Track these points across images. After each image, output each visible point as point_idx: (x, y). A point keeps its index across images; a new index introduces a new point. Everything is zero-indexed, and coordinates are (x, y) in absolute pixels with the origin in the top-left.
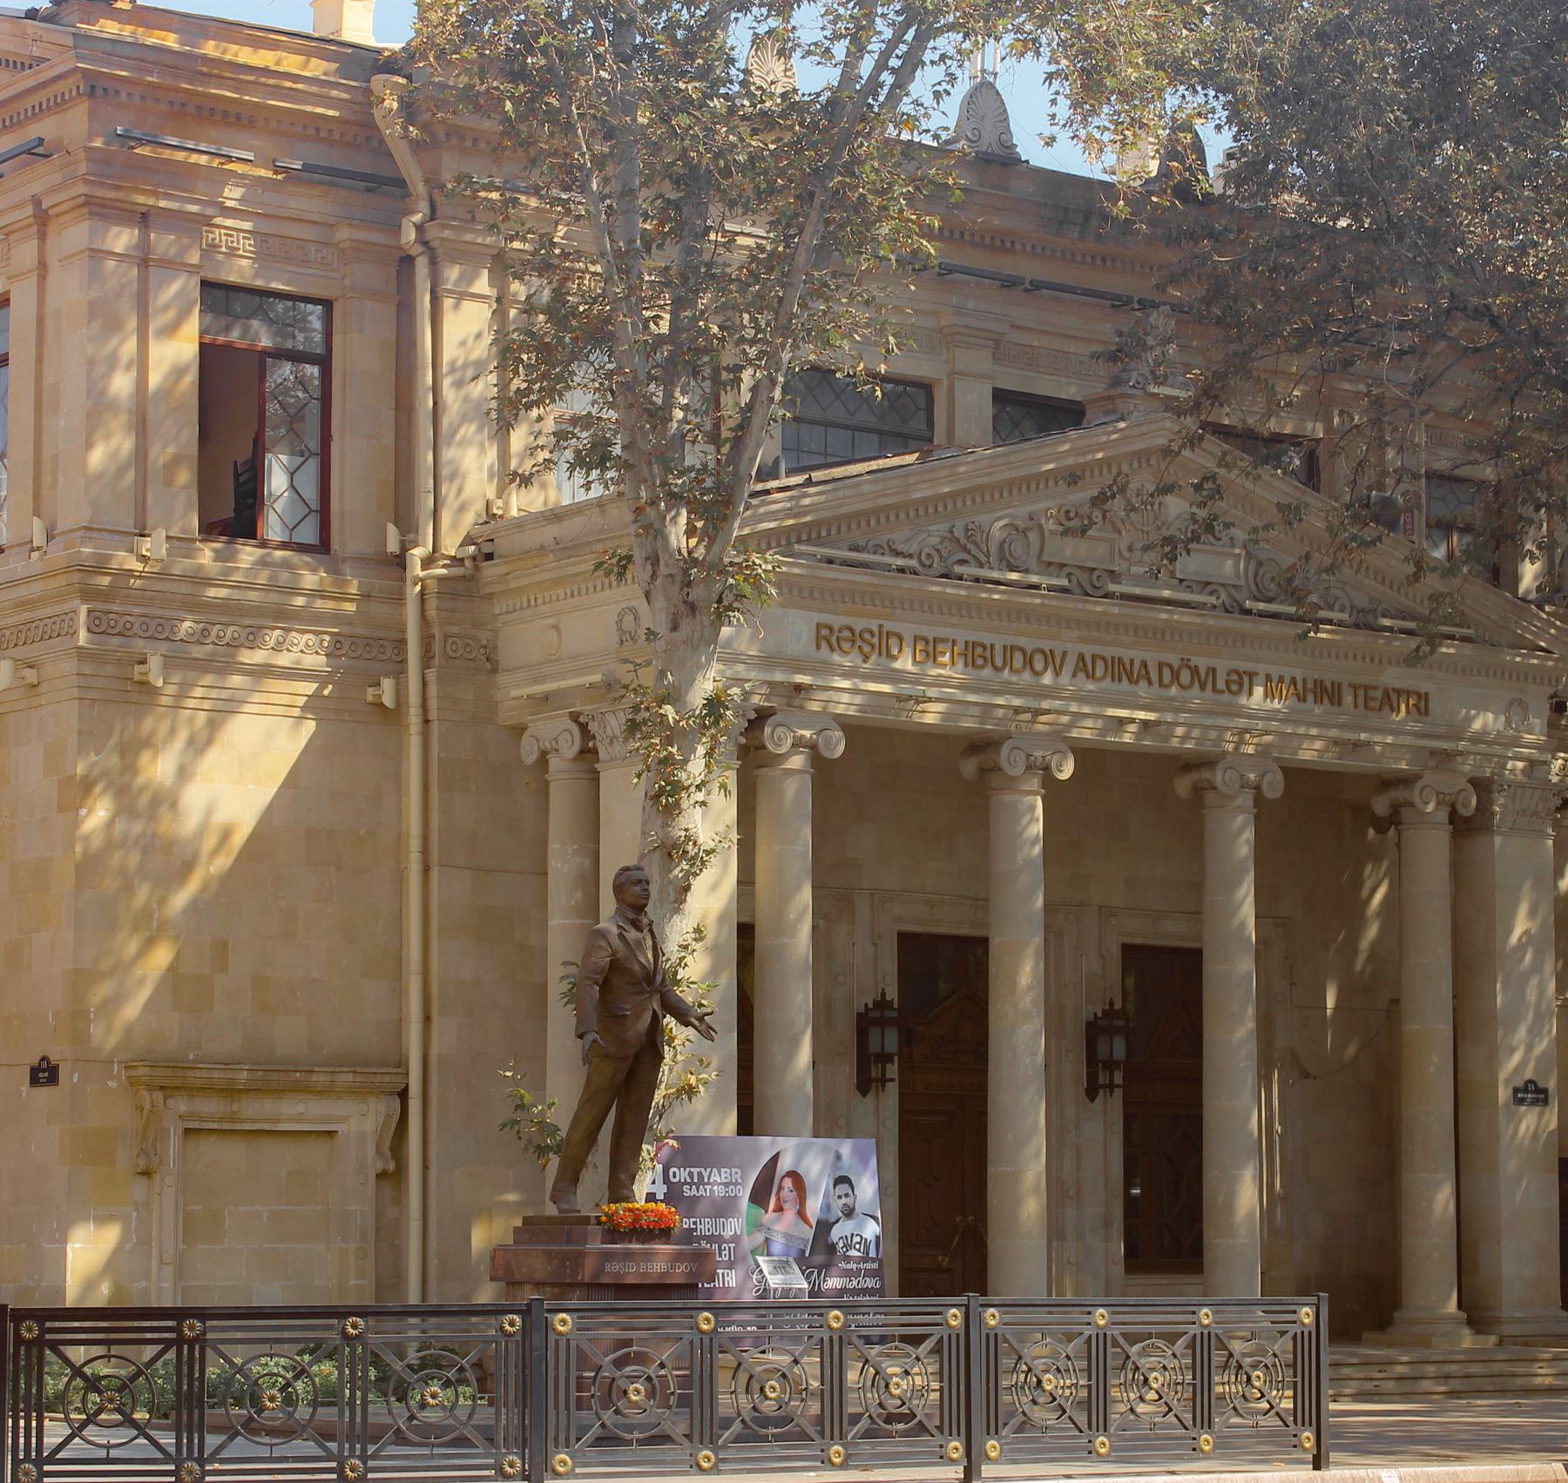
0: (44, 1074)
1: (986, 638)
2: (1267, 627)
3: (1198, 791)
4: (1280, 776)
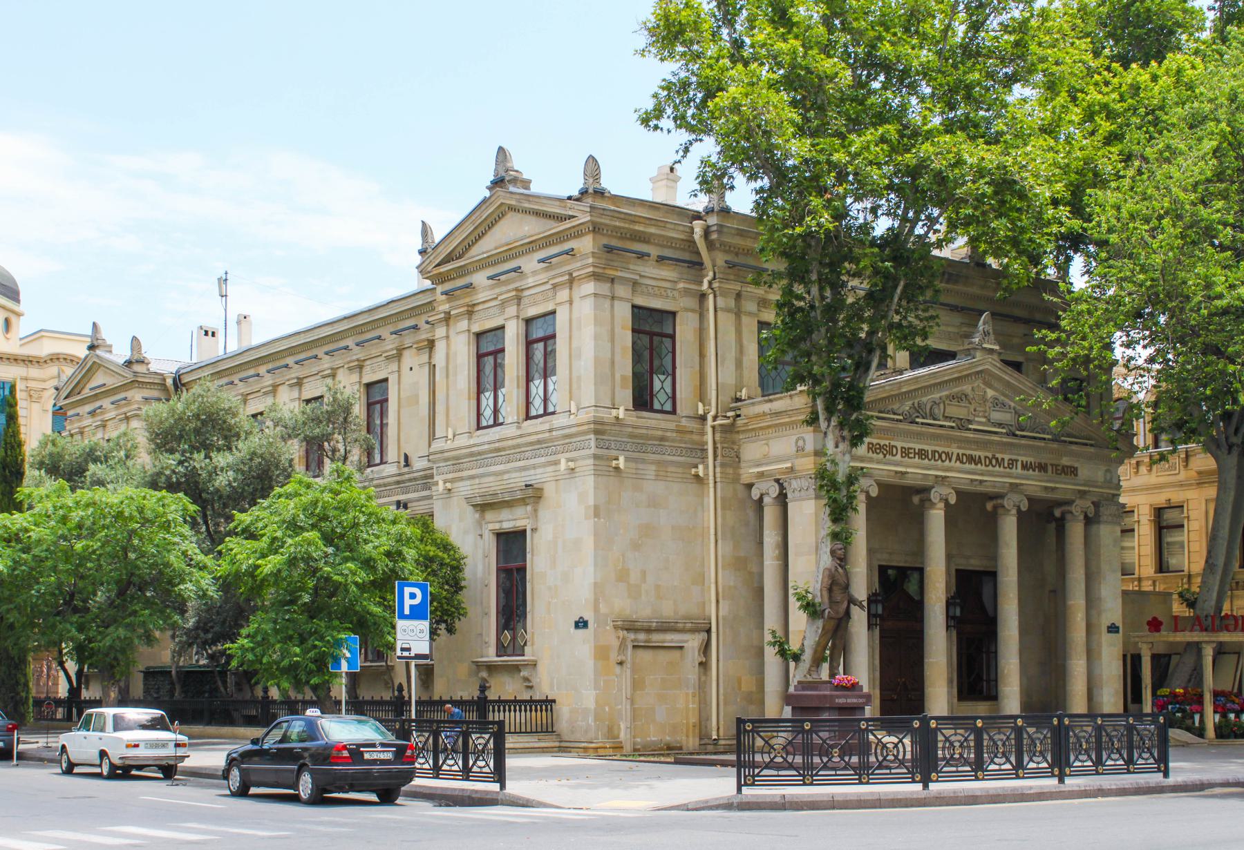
0: (581, 624)
1: (926, 447)
2: (1023, 442)
3: (995, 508)
4: (1026, 502)
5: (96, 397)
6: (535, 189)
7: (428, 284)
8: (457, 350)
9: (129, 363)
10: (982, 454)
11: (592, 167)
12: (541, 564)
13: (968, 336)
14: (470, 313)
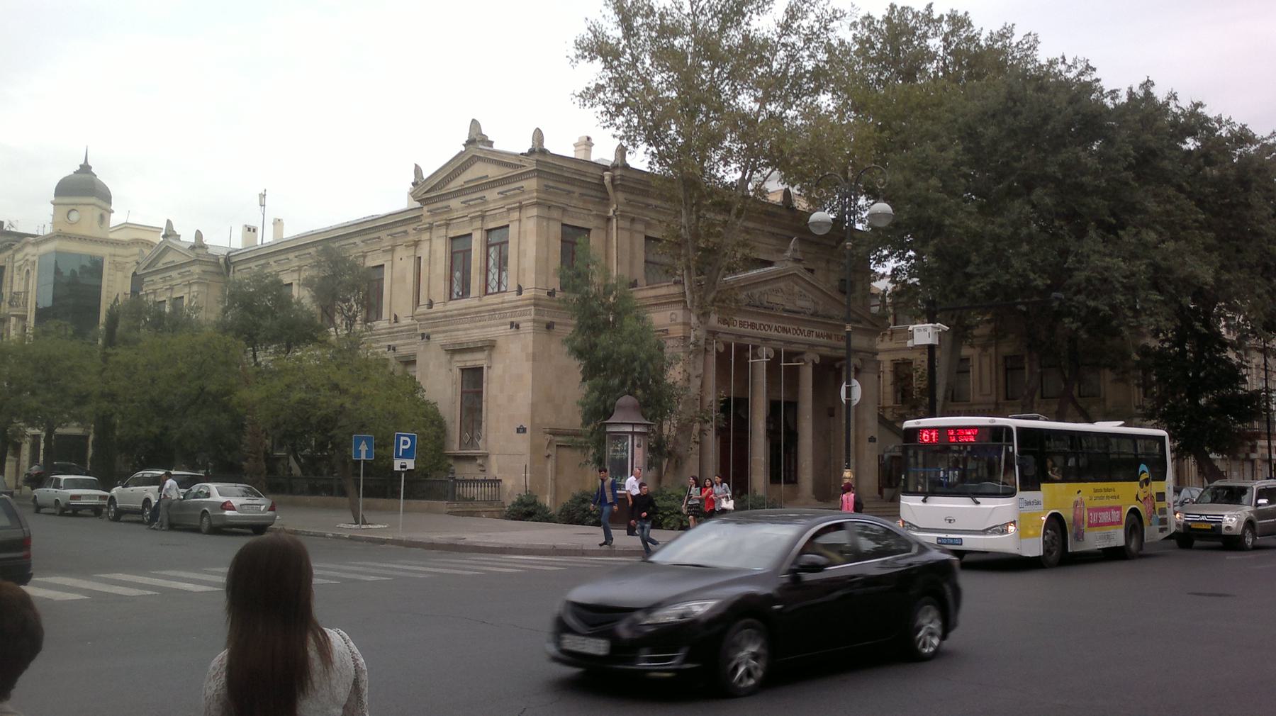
0: (521, 430)
5: (167, 269)
6: (496, 147)
7: (418, 205)
8: (437, 250)
9: (193, 248)
10: (792, 327)
11: (538, 135)
12: (492, 389)
13: (784, 251)
14: (447, 225)
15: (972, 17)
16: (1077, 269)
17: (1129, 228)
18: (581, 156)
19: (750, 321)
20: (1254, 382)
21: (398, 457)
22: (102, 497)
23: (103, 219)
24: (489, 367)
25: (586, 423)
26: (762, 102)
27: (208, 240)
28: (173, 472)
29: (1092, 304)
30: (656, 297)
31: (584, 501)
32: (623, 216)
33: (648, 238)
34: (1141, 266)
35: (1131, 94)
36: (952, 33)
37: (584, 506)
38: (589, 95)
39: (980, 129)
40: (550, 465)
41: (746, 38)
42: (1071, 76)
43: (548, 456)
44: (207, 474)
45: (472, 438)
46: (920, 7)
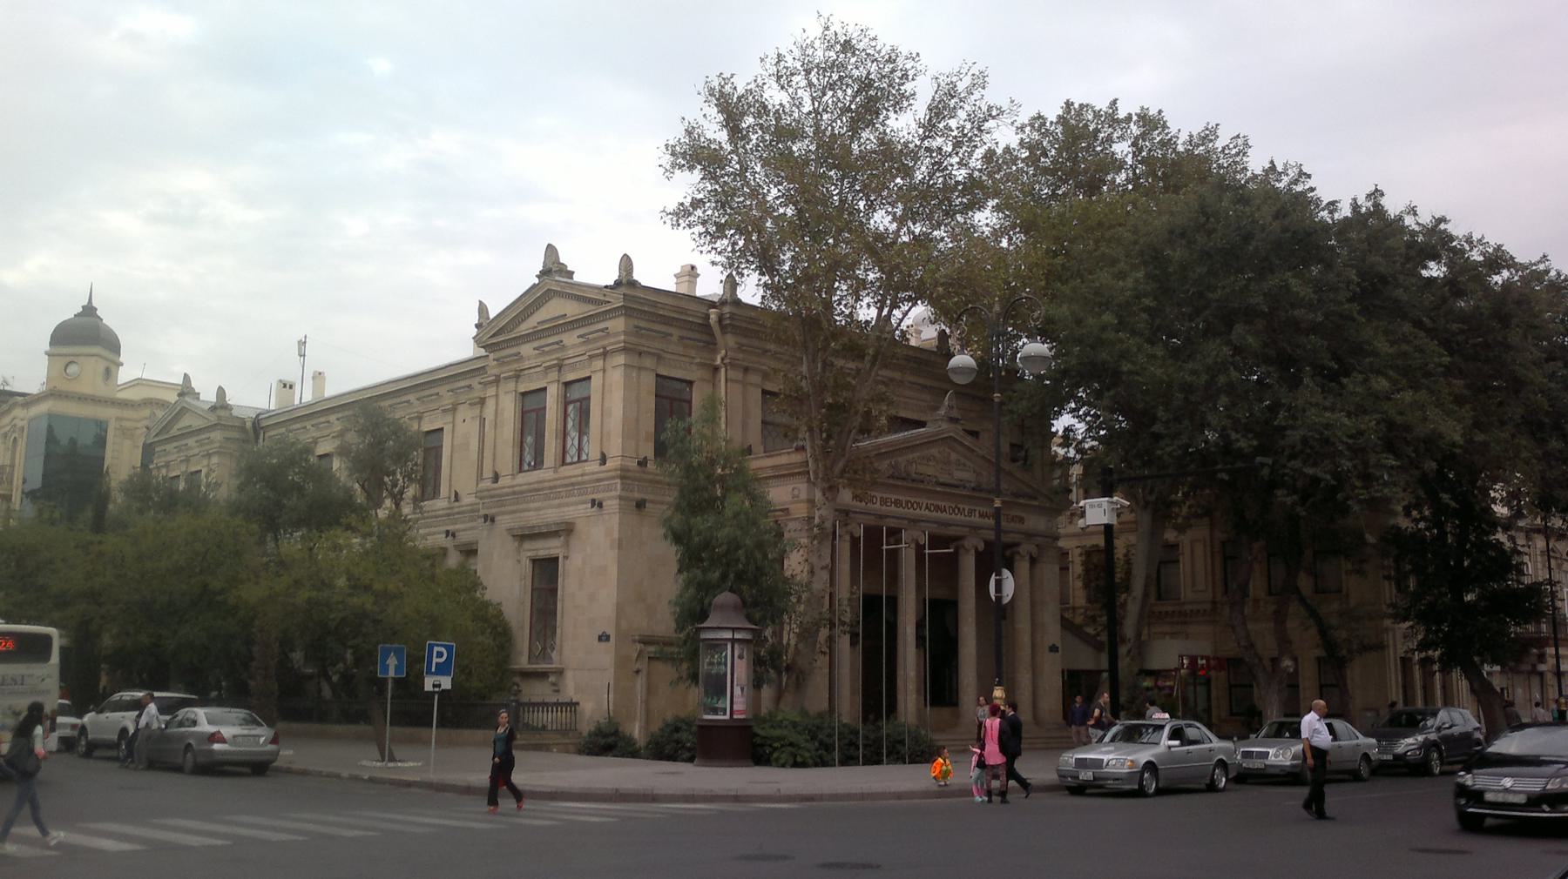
0: (604, 638)
6: (577, 278)
7: (482, 352)
9: (213, 408)
10: (947, 504)
11: (626, 263)
12: (569, 585)
13: (936, 409)
15: (1167, 116)
16: (1292, 428)
17: (1355, 374)
18: (683, 290)
19: (894, 497)
20: (1534, 570)
21: (429, 672)
22: (74, 726)
23: (109, 374)
24: (566, 558)
25: (680, 629)
26: (901, 221)
27: (232, 399)
28: (156, 694)
29: (1309, 471)
30: (773, 467)
31: (677, 729)
32: (732, 365)
33: (765, 392)
34: (1369, 422)
35: (1355, 207)
36: (1143, 136)
37: (676, 736)
38: (681, 214)
39: (1168, 252)
40: (640, 683)
41: (882, 141)
42: (1281, 185)
43: (638, 672)
44: (220, 695)
45: (544, 649)
46: (1102, 105)
